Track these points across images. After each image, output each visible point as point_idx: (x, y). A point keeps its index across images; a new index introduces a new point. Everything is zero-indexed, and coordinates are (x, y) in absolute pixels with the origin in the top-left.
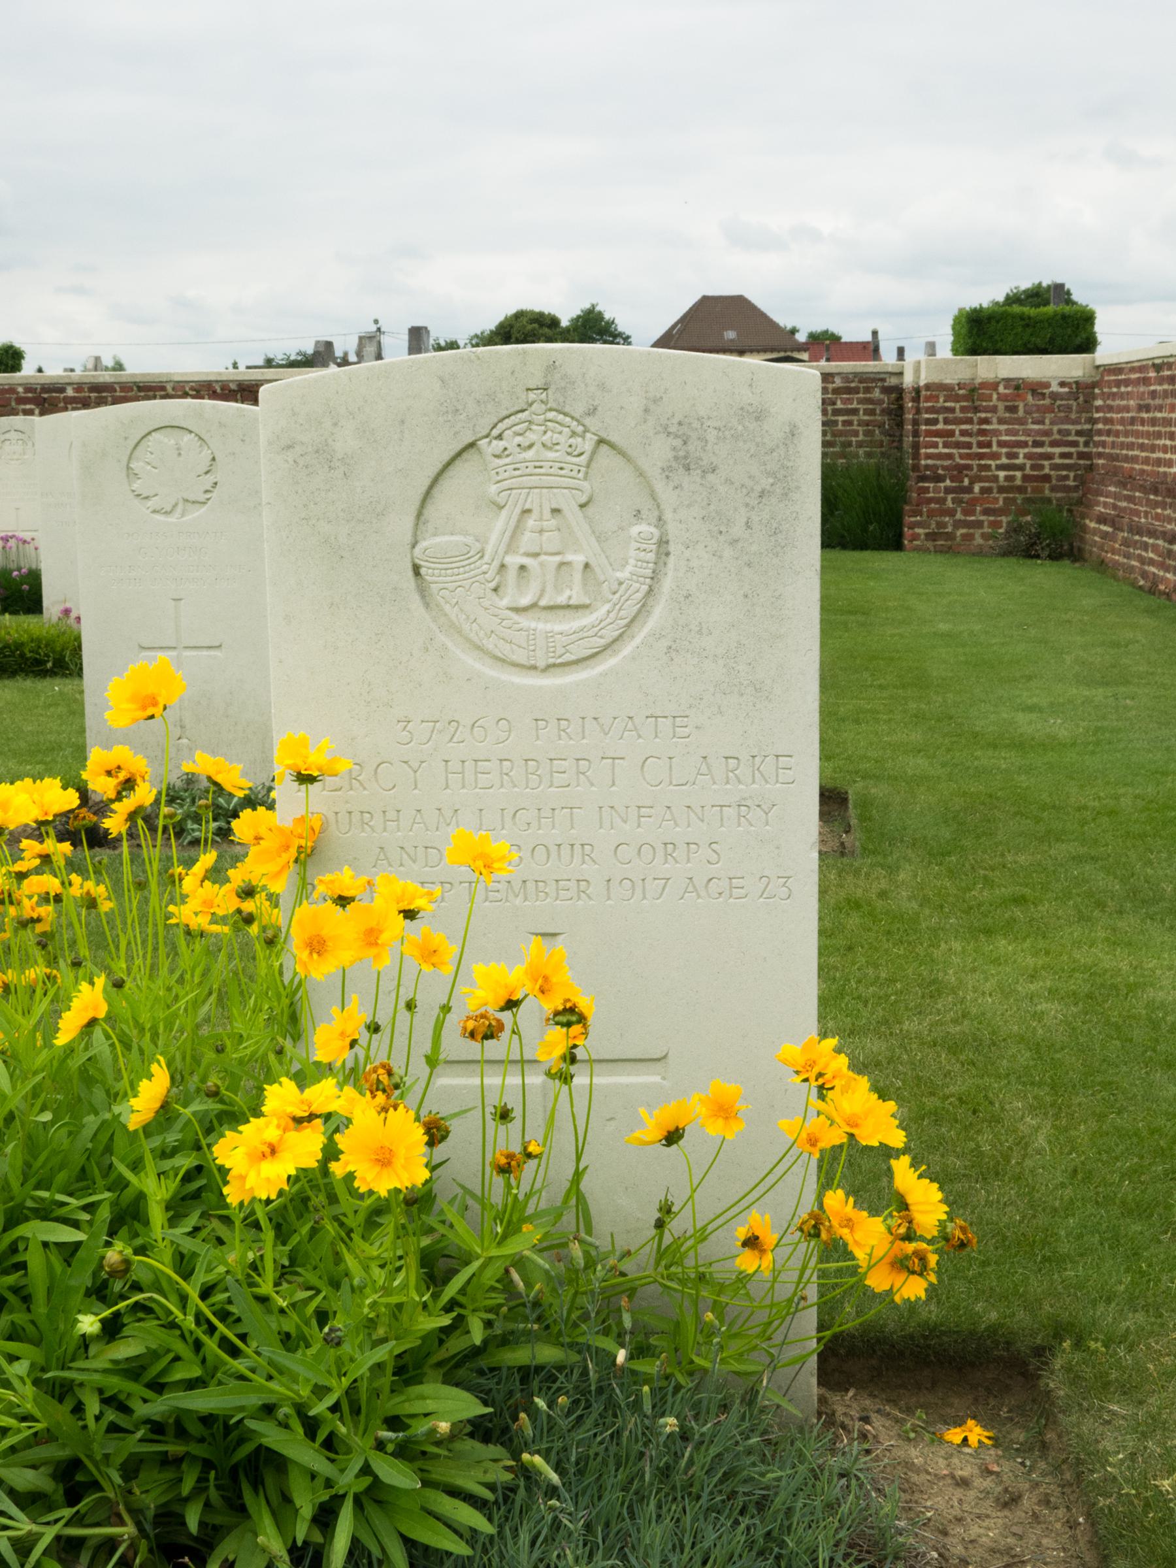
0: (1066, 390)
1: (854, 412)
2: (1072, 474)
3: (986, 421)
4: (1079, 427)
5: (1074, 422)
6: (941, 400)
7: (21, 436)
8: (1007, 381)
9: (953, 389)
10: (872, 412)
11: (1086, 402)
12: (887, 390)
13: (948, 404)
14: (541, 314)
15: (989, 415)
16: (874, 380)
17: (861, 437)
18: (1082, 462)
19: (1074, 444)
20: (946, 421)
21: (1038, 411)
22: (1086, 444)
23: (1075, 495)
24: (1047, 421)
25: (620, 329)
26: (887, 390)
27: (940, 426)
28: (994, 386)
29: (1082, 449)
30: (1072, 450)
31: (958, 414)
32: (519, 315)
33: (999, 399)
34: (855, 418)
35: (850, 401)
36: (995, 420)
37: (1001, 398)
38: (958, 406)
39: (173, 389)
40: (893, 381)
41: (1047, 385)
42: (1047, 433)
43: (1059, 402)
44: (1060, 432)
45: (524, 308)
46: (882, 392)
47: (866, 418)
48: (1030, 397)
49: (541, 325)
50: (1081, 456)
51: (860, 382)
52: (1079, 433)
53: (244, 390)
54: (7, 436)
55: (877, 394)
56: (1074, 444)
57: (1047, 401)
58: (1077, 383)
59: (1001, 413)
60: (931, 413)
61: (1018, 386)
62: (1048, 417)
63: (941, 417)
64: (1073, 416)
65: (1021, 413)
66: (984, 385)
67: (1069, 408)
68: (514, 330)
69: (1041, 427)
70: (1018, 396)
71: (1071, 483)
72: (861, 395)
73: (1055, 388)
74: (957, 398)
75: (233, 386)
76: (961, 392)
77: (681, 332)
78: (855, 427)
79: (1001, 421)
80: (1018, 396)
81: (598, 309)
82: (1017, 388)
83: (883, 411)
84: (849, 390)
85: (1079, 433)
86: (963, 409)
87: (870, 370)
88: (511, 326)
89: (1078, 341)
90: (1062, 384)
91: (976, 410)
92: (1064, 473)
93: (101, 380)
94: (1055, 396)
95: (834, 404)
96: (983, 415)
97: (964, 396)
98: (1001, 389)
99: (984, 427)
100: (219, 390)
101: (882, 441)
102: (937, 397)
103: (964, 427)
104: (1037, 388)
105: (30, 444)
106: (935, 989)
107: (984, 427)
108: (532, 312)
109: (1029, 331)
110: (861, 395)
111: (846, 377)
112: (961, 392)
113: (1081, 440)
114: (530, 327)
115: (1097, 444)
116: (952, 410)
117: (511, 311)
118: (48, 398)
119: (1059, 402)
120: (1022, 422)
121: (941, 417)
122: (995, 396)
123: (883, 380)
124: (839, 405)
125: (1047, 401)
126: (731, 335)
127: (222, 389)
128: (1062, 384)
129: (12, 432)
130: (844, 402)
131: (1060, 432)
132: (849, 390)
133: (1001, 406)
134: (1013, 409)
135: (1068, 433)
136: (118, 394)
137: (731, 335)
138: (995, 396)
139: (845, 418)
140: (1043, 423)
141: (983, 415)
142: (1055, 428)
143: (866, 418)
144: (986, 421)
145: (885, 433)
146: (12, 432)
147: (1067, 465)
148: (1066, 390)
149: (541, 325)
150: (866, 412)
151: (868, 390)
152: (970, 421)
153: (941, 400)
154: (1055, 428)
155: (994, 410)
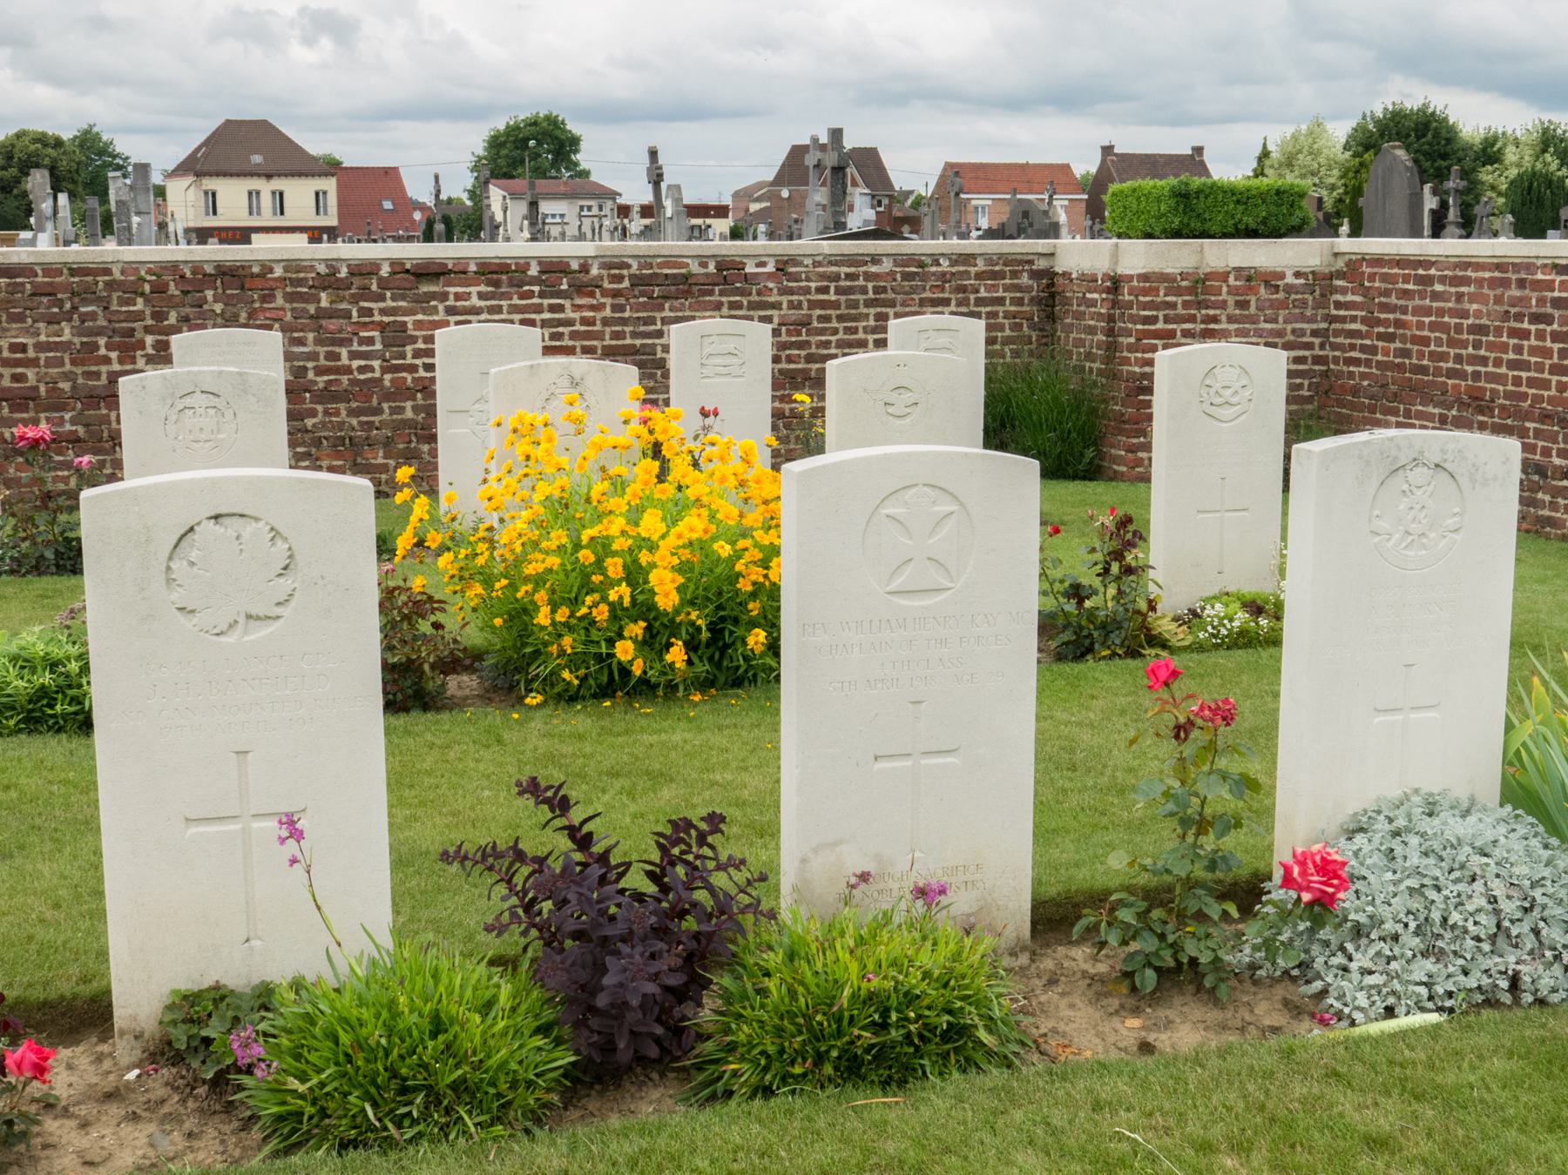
0: (1302, 281)
1: (1000, 301)
2: (1306, 383)
3: (1215, 319)
4: (1315, 326)
5: (1312, 320)
6: (1162, 293)
7: (213, 401)
8: (1238, 270)
9: (1175, 280)
10: (1020, 302)
11: (1323, 295)
12: (1036, 275)
13: (1168, 299)
14: (44, 134)
15: (1218, 312)
16: (1021, 262)
17: (1008, 332)
18: (1317, 368)
19: (1309, 346)
20: (1167, 320)
21: (1271, 307)
22: (1322, 346)
23: (1310, 407)
24: (1281, 319)
25: (118, 150)
27: (1160, 325)
28: (1224, 277)
29: (1318, 352)
30: (1307, 353)
31: (1180, 311)
33: (1229, 293)
34: (1001, 309)
35: (994, 288)
36: (1224, 318)
37: (1232, 291)
38: (1180, 300)
39: (123, 273)
40: (1041, 264)
41: (1282, 276)
42: (1280, 333)
43: (1293, 296)
47: (1013, 308)
48: (1262, 290)
50: (1318, 360)
52: (1314, 333)
53: (224, 274)
54: (188, 401)
55: (1025, 279)
56: (1309, 346)
57: (1281, 295)
58: (1313, 273)
59: (1232, 310)
61: (1252, 278)
62: (1282, 313)
63: (1161, 314)
64: (1308, 313)
65: (1253, 310)
66: (1210, 276)
67: (1305, 302)
68: (16, 150)
70: (1250, 288)
71: (1306, 393)
72: (1007, 281)
73: (1290, 279)
74: (1179, 291)
75: (209, 269)
76: (1184, 283)
79: (1231, 319)
80: (1250, 288)
82: (1249, 279)
83: (1032, 300)
85: (1314, 333)
86: (1186, 305)
88: (13, 146)
89: (1295, 221)
91: (1200, 305)
92: (1298, 381)
93: (15, 260)
94: (1289, 289)
95: (977, 291)
96: (1211, 312)
99: (1212, 326)
100: (188, 274)
101: (1030, 337)
102: (1157, 290)
104: (1270, 279)
105: (229, 414)
107: (1212, 326)
110: (1007, 281)
112: (1184, 283)
113: (1317, 341)
114: (32, 147)
115: (1335, 347)
116: (1173, 306)
118: (1288, 445)
119: (1293, 296)
121: (1161, 314)
122: (1225, 289)
123: (1031, 262)
124: (983, 293)
125: (1281, 295)
126: (257, 159)
127: (193, 273)
128: (1297, 275)
130: (989, 289)
131: (1294, 331)
133: (1231, 300)
134: (1243, 305)
135: (1302, 333)
136: (39, 279)
137: (257, 159)
138: (1225, 289)
139: (988, 309)
140: (1275, 321)
141: (1211, 312)
142: (1289, 327)
143: (1013, 308)
144: (1215, 319)
147: (1302, 371)
148: (1302, 281)
149: (45, 145)
150: (1014, 301)
151: (1015, 274)
152: (1192, 319)
153: (1162, 293)
154: (1289, 327)
155: (1223, 305)
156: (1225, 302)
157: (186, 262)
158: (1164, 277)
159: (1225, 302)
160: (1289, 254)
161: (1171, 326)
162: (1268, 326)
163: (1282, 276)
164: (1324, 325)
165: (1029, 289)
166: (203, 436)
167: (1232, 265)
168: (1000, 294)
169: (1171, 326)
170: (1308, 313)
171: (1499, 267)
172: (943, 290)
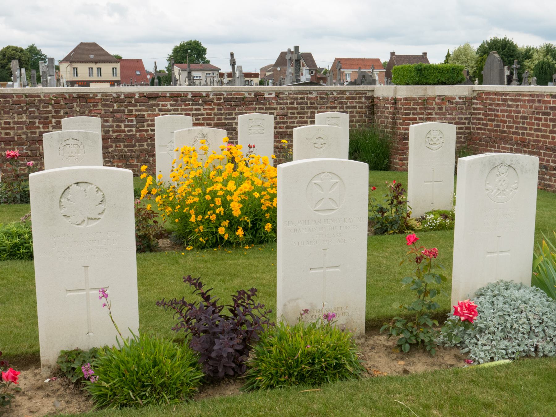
0: (462, 100)
2: (463, 136)
3: (431, 114)
4: (466, 116)
5: (465, 114)
6: (412, 104)
7: (76, 142)
8: (439, 96)
9: (416, 100)
10: (362, 107)
11: (469, 105)
12: (367, 98)
13: (414, 106)
14: (17, 47)
15: (432, 111)
16: (362, 94)
17: (357, 118)
18: (467, 131)
19: (464, 123)
21: (450, 109)
22: (468, 123)
24: (454, 114)
25: (43, 53)
26: (367, 98)
27: (411, 116)
28: (434, 99)
30: (463, 126)
31: (418, 111)
32: (8, 48)
34: (355, 110)
36: (434, 113)
38: (418, 107)
39: (44, 97)
40: (369, 94)
41: (454, 98)
42: (454, 119)
43: (458, 106)
44: (458, 118)
45: (10, 45)
46: (365, 99)
47: (359, 110)
48: (447, 103)
49: (17, 51)
50: (467, 128)
51: (356, 94)
52: (466, 119)
53: (80, 97)
54: (67, 142)
55: (363, 100)
56: (464, 123)
57: (454, 105)
58: (465, 97)
60: (408, 110)
61: (444, 99)
62: (455, 112)
63: (411, 112)
64: (464, 112)
65: (444, 110)
66: (429, 98)
67: (462, 108)
68: (7, 53)
69: (451, 116)
70: (443, 103)
72: (357, 100)
73: (457, 100)
74: (418, 104)
75: (75, 95)
76: (420, 101)
77: (74, 55)
78: (355, 114)
79: (436, 114)
80: (443, 103)
81: (35, 46)
82: (443, 100)
83: (366, 107)
84: (353, 98)
85: (466, 119)
86: (420, 109)
87: (361, 89)
90: (460, 98)
91: (425, 109)
92: (460, 136)
93: (6, 92)
94: (457, 103)
95: (347, 104)
96: (429, 111)
97: (421, 103)
98: (436, 100)
99: (430, 116)
100: (67, 97)
102: (410, 103)
103: (420, 116)
104: (450, 100)
105: (82, 147)
106: (29, 243)
107: (430, 116)
108: (14, 47)
109: (440, 74)
110: (357, 100)
111: (351, 92)
112: (420, 101)
113: (467, 122)
114: (12, 52)
115: (473, 124)
116: (416, 109)
117: (5, 46)
119: (458, 106)
120: (444, 114)
121: (411, 112)
122: (434, 103)
123: (365, 93)
124: (349, 104)
125: (454, 105)
126: (92, 56)
127: (69, 97)
128: (460, 98)
129: (71, 140)
130: (350, 103)
131: (458, 118)
132: (353, 98)
133: (436, 107)
134: (441, 109)
135: (462, 119)
137: (92, 56)
138: (434, 103)
139: (351, 110)
140: (452, 114)
141: (429, 111)
142: (457, 117)
143: (359, 110)
144: (431, 114)
145: (366, 116)
146: (71, 140)
148: (462, 100)
149: (17, 51)
150: (360, 107)
151: (360, 98)
152: (422, 114)
153: (412, 104)
154: (457, 117)
155: (433, 109)
158: (413, 99)
162: (450, 116)
163: (454, 98)
164: (469, 116)
165: (365, 103)
170: (464, 112)
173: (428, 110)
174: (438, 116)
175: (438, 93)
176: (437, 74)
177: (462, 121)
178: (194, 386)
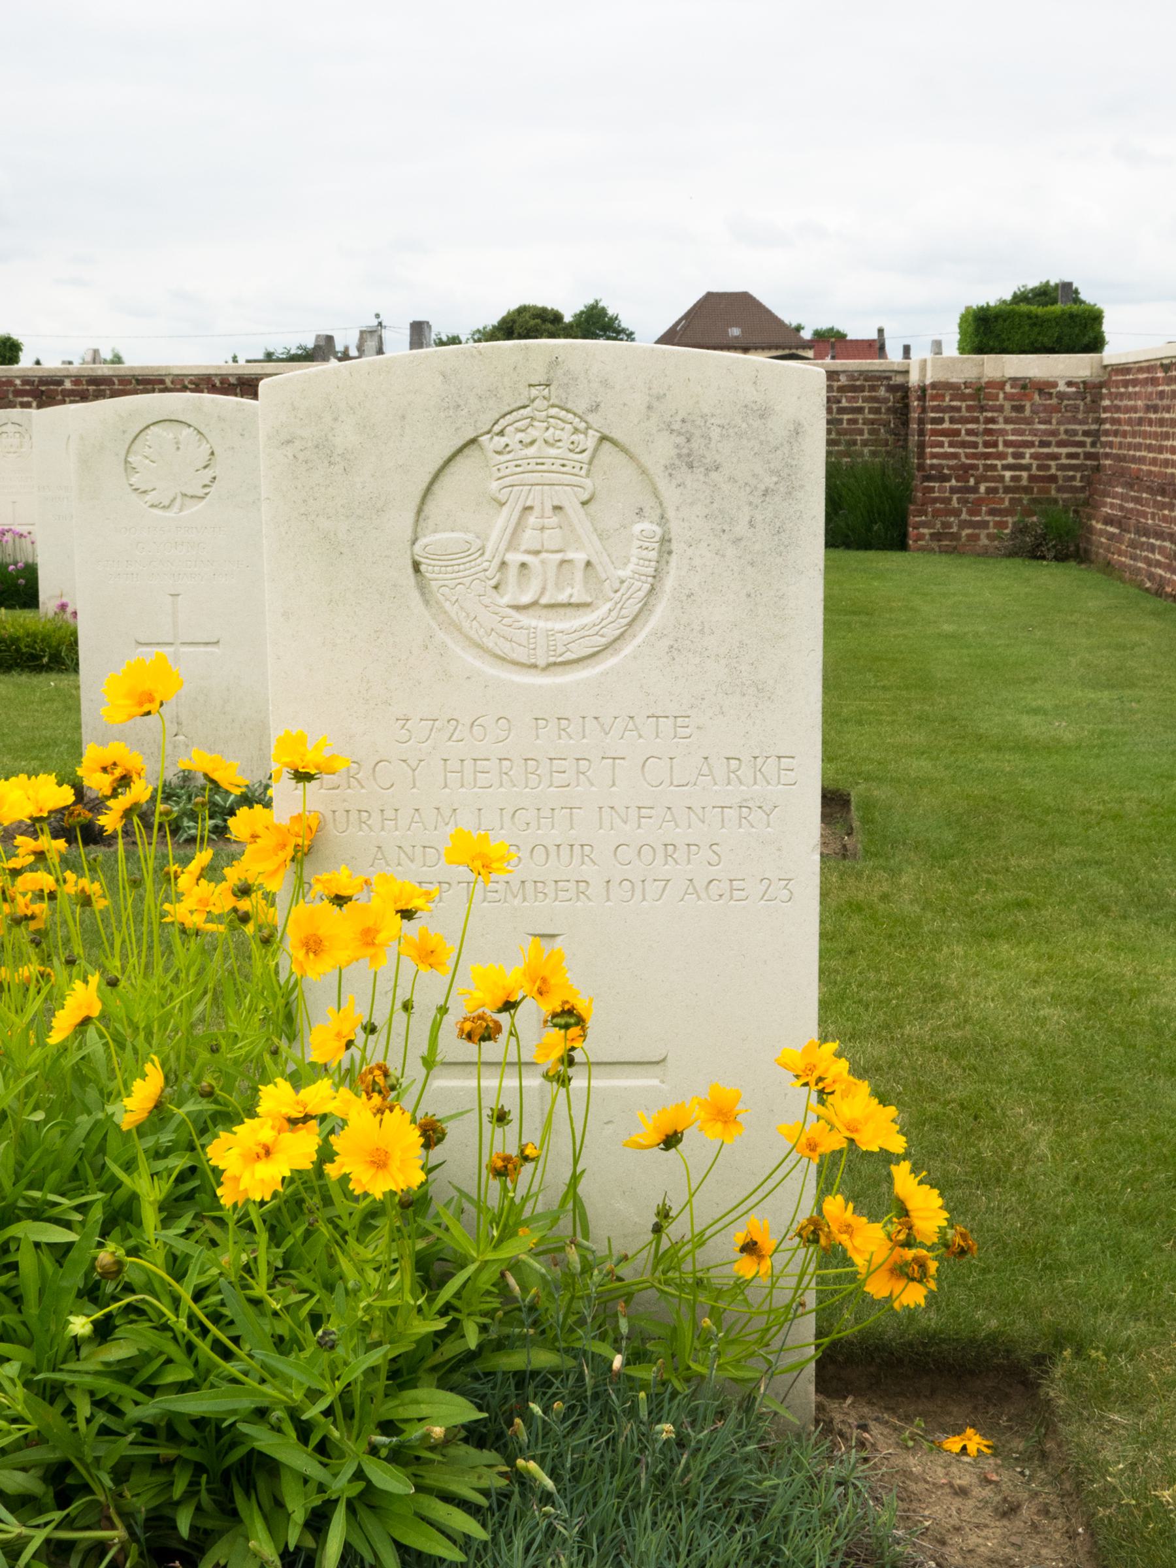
0: (1074, 389)
1: (860, 410)
2: (1078, 475)
4: (1086, 427)
5: (1081, 423)
6: (947, 399)
8: (1014, 381)
9: (959, 388)
10: (877, 411)
11: (1093, 401)
12: (892, 389)
13: (954, 403)
14: (544, 310)
15: (995, 414)
16: (879, 378)
17: (866, 436)
18: (1088, 462)
19: (1081, 444)
20: (952, 421)
21: (1045, 411)
22: (1093, 444)
23: (1082, 495)
24: (1054, 421)
25: (624, 325)
26: (892, 389)
27: (946, 425)
28: (1001, 385)
29: (1089, 449)
30: (1079, 450)
31: (964, 413)
32: (522, 310)
33: (1005, 398)
34: (860, 417)
35: (855, 399)
36: (1001, 420)
37: (1008, 397)
38: (964, 405)
39: (172, 382)
40: (899, 380)
41: (1054, 385)
42: (1054, 433)
43: (1066, 402)
45: (527, 303)
46: (887, 391)
48: (1036, 397)
49: (544, 321)
50: (1088, 456)
51: (866, 380)
52: (1086, 433)
53: (243, 384)
55: (882, 392)
56: (1081, 444)
57: (1054, 401)
58: (1084, 383)
59: (1008, 412)
60: (937, 412)
61: (1025, 386)
62: (1055, 417)
63: (947, 416)
64: (1080, 416)
65: (1027, 413)
66: (990, 384)
67: (1077, 408)
69: (1048, 427)
70: (1025, 395)
71: (1078, 484)
73: (1062, 387)
74: (963, 398)
75: (233, 380)
76: (967, 391)
77: (685, 328)
78: (860, 426)
79: (1007, 421)
80: (1025, 395)
81: (601, 304)
82: (1024, 387)
83: (888, 410)
84: (854, 389)
85: (1086, 433)
86: (969, 408)
87: (876, 368)
88: (514, 322)
91: (983, 409)
92: (1071, 473)
94: (1062, 396)
95: (839, 402)
96: (989, 415)
98: (1008, 388)
100: (218, 384)
101: (887, 440)
102: (943, 396)
103: (970, 426)
104: (1043, 388)
105: (27, 437)
106: (937, 993)
108: (535, 307)
110: (866, 394)
111: (851, 375)
112: (967, 391)
113: (1088, 440)
114: (532, 322)
116: (958, 409)
117: (514, 306)
119: (1066, 402)
120: (1028, 421)
121: (947, 416)
122: (1001, 396)
123: (889, 378)
124: (844, 403)
125: (1054, 401)
126: (735, 332)
128: (1070, 384)
129: (10, 425)
130: (849, 400)
131: (1066, 432)
132: (854, 389)
133: (1007, 405)
134: (1019, 409)
137: (735, 332)
138: (1001, 396)
140: (1049, 422)
141: (989, 415)
142: (1062, 428)
144: (993, 421)
146: (10, 425)
148: (1074, 389)
149: (544, 321)
150: (871, 410)
151: (873, 388)
152: (976, 420)
153: (947, 399)
154: (1062, 428)
155: (1000, 409)
156: (1002, 406)
157: (216, 375)
158: (948, 386)
159: (1002, 406)
160: (1061, 366)
161: (956, 426)
162: (1043, 427)
163: (1054, 385)
164: (1094, 427)
165: (886, 400)
166: (12, 450)
167: (1008, 375)
168: (860, 404)
169: (956, 426)
170: (1080, 416)
171: (1149, 369)
172: (1050, 423)
173: (986, 411)
174: (1012, 426)
175: (1010, 372)
176: (1027, 328)
177: (1077, 439)
178: (189, 828)
